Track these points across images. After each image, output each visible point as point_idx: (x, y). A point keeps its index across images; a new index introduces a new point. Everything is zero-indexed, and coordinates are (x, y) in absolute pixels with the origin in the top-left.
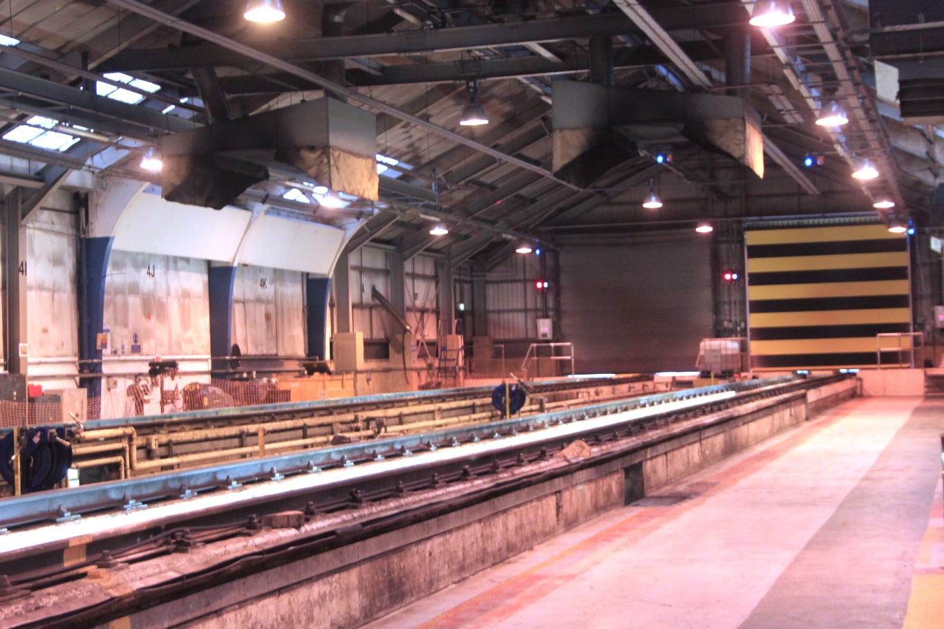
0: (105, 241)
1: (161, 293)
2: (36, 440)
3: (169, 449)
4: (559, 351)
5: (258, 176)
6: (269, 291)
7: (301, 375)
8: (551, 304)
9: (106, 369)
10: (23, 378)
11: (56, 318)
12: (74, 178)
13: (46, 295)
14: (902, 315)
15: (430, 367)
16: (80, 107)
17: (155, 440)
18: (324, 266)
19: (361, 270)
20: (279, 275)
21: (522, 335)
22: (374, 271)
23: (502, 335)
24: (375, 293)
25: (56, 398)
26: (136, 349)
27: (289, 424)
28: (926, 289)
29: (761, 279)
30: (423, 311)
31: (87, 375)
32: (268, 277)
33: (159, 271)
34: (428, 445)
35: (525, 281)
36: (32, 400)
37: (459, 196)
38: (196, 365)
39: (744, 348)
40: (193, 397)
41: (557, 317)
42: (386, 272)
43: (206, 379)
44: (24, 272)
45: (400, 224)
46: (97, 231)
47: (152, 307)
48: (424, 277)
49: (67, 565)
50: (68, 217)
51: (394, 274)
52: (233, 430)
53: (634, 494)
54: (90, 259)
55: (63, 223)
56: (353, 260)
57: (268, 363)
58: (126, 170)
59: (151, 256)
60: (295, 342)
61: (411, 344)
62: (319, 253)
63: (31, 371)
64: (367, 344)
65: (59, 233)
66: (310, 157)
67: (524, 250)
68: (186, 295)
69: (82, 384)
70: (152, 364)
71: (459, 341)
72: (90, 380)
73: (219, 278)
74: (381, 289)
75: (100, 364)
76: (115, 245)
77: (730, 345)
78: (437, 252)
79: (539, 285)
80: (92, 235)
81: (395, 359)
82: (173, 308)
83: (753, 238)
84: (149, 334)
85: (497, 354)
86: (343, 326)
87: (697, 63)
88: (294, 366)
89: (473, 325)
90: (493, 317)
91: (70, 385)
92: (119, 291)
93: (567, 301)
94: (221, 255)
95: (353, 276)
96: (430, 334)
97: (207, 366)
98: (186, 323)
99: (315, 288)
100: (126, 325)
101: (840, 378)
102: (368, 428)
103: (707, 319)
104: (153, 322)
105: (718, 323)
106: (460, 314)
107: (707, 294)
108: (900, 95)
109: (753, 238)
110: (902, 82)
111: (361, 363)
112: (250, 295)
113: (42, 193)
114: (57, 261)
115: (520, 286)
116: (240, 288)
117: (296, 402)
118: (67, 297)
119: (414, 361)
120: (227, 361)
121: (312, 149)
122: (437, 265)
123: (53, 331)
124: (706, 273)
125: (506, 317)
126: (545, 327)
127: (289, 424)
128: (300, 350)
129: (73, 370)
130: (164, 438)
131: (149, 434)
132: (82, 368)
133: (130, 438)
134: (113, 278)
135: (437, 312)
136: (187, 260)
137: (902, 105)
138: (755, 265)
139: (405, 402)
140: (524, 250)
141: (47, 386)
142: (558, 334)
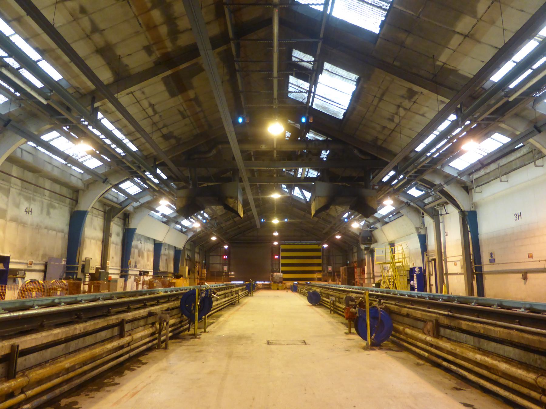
1: (143, 249)
8: (227, 262)
10: (108, 273)
11: (116, 254)
14: (320, 268)
18: (180, 246)
26: (136, 267)
28: (325, 262)
31: (124, 274)
34: (113, 297)
35: (220, 256)
36: (109, 281)
41: (229, 265)
42: (190, 250)
44: (111, 236)
46: (132, 226)
50: (122, 220)
54: (128, 236)
55: (120, 222)
57: (166, 273)
60: (171, 269)
65: (119, 226)
68: (149, 251)
69: (122, 277)
70: (140, 272)
72: (124, 275)
73: (158, 246)
75: (128, 270)
76: (137, 232)
79: (225, 257)
80: (130, 227)
84: (139, 263)
87: (236, 209)
90: (211, 265)
91: (117, 277)
94: (160, 238)
98: (148, 260)
102: (232, 295)
104: (140, 258)
105: (272, 269)
116: (163, 251)
118: (119, 247)
121: (232, 198)
123: (115, 258)
125: (214, 265)
126: (226, 268)
128: (172, 271)
129: (119, 272)
131: (411, 301)
132: (122, 271)
135: (199, 263)
138: (283, 254)
141: (113, 277)
142: (229, 270)
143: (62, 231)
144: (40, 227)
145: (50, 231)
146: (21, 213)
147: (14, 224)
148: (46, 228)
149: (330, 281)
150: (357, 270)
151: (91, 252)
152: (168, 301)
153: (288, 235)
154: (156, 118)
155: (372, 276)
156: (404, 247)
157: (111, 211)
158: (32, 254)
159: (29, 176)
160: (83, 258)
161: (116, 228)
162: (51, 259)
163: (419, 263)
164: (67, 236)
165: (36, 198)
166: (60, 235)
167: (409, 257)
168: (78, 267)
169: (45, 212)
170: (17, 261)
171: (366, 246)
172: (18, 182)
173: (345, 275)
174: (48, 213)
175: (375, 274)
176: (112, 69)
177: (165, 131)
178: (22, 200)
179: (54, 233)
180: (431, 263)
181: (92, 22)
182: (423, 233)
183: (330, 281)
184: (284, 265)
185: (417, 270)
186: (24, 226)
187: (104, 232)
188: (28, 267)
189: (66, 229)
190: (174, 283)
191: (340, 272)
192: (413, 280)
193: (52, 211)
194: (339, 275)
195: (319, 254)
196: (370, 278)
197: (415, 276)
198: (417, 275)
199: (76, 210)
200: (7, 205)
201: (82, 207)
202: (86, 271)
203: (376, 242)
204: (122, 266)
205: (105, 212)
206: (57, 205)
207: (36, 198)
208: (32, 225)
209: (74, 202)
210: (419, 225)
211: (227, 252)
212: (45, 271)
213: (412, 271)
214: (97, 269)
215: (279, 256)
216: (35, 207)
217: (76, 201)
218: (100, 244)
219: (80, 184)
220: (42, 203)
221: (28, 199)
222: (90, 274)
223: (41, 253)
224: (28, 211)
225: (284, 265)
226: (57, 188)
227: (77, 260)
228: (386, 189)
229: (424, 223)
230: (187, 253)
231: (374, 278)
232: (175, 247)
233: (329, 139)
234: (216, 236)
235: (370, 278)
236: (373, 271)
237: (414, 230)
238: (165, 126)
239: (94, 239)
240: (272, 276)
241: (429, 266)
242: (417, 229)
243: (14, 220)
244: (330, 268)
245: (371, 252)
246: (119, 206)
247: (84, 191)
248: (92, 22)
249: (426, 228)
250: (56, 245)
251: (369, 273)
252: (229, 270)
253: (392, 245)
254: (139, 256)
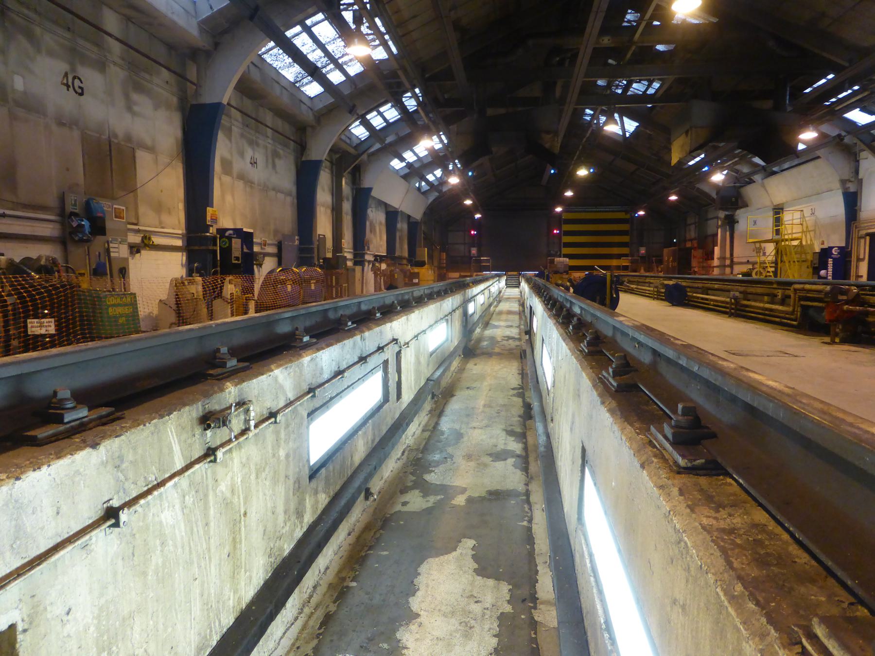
14: (625, 251)
29: (567, 233)
46: (366, 184)
54: (362, 199)
68: (381, 223)
75: (364, 254)
80: (362, 186)
98: (381, 237)
104: (372, 236)
121: (548, 132)
126: (474, 251)
138: (566, 227)
142: (480, 254)
143: (290, 194)
147: (240, 184)
149: (642, 271)
150: (697, 253)
151: (323, 226)
153: (589, 192)
155: (728, 262)
156: (807, 213)
163: (837, 240)
167: (814, 231)
169: (270, 166)
171: (727, 213)
173: (673, 261)
174: (274, 166)
175: (735, 260)
180: (862, 241)
182: (852, 188)
183: (642, 271)
184: (567, 245)
185: (834, 252)
186: (251, 187)
188: (262, 248)
189: (294, 190)
190: (418, 273)
191: (662, 256)
192: (826, 268)
193: (277, 161)
194: (660, 262)
195: (625, 227)
196: (725, 266)
197: (830, 261)
198: (835, 260)
199: (303, 159)
200: (231, 154)
203: (746, 205)
206: (281, 152)
207: (260, 142)
210: (847, 173)
213: (825, 253)
217: (302, 147)
219: (308, 116)
225: (567, 245)
226: (280, 124)
228: (815, 109)
229: (857, 172)
231: (731, 266)
232: (409, 217)
233: (368, 6)
235: (725, 266)
236: (732, 254)
237: (837, 185)
240: (552, 262)
241: (858, 245)
242: (843, 182)
243: (241, 177)
244: (643, 251)
245: (731, 222)
246: (352, 151)
247: (313, 127)
249: (860, 182)
251: (722, 258)
252: (480, 254)
253: (778, 210)
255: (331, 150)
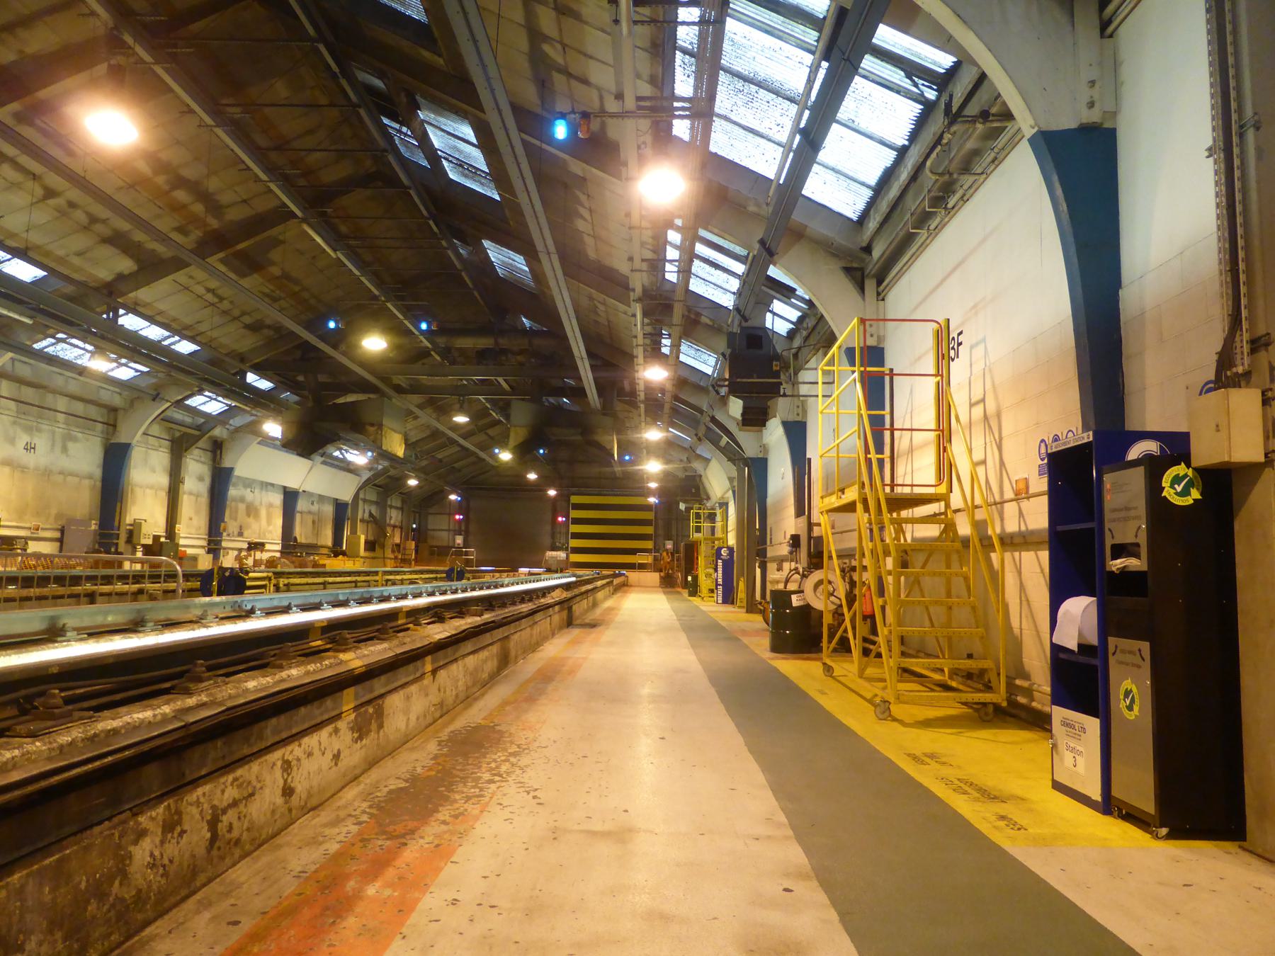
0: (231, 469)
1: (257, 503)
2: (227, 574)
3: (288, 588)
4: (467, 553)
5: (333, 439)
6: (315, 508)
7: (329, 556)
9: (224, 544)
10: (177, 545)
11: (197, 512)
12: (218, 432)
13: (193, 498)
14: (649, 545)
15: (396, 558)
16: (236, 389)
17: (282, 581)
18: (346, 496)
19: (365, 501)
20: (322, 498)
21: (445, 544)
22: (371, 502)
23: (434, 544)
24: (371, 515)
25: (194, 559)
26: (241, 534)
27: (349, 579)
28: (661, 532)
29: (577, 521)
30: (394, 527)
32: (315, 499)
33: (257, 491)
35: (449, 514)
37: (424, 463)
38: (274, 547)
39: (567, 557)
40: (271, 563)
42: (376, 503)
43: (278, 555)
45: (389, 477)
46: (226, 463)
47: (252, 510)
48: (396, 508)
49: (400, 622)
51: (382, 504)
52: (320, 580)
53: (569, 623)
54: (220, 480)
56: (361, 496)
57: (312, 548)
58: (252, 429)
59: (254, 481)
60: (327, 538)
61: (389, 543)
62: (345, 489)
63: (182, 542)
64: (366, 542)
65: (203, 463)
66: (371, 429)
67: (453, 497)
68: (270, 505)
69: (209, 552)
71: (413, 545)
73: (290, 497)
74: (373, 512)
76: (237, 473)
77: (561, 555)
78: (407, 495)
81: (378, 552)
82: (263, 513)
83: (575, 499)
85: (432, 553)
86: (354, 531)
88: (325, 551)
89: (420, 536)
91: (201, 552)
92: (235, 500)
93: (472, 528)
94: (293, 484)
95: (361, 503)
96: (397, 540)
97: (279, 547)
98: (269, 522)
99: (340, 507)
100: (236, 520)
101: (615, 576)
103: (547, 540)
104: (251, 520)
106: (413, 530)
107: (548, 528)
108: (743, 415)
109: (575, 499)
110: (745, 408)
111: (362, 552)
112: (305, 509)
113: (198, 438)
114: (201, 479)
115: (446, 517)
116: (302, 505)
117: (328, 569)
118: (204, 500)
119: (389, 554)
120: (289, 544)
121: (372, 425)
122: (403, 502)
124: (549, 516)
126: (459, 540)
127: (349, 579)
128: (330, 543)
129: (204, 543)
130: (286, 581)
132: (210, 542)
133: (270, 579)
134: (233, 492)
135: (401, 528)
136: (272, 485)
137: (744, 420)
138: (575, 514)
139: (404, 573)
140: (453, 497)
141: (190, 551)
142: (466, 545)
144: (51, 471)
145: (69, 478)
146: (18, 451)
148: (61, 473)
151: (145, 510)
152: (461, 615)
154: (225, 305)
157: (183, 439)
158: (38, 514)
159: (28, 393)
160: (129, 520)
161: (196, 471)
162: (72, 521)
164: (99, 484)
165: (44, 427)
166: (86, 482)
168: (118, 535)
170: (14, 524)
172: (12, 404)
174: (65, 449)
176: (132, 257)
177: (247, 320)
178: (19, 431)
179: (77, 479)
181: (87, 213)
187: (171, 476)
189: (98, 473)
193: (70, 445)
198: (724, 561)
201: (122, 438)
202: (135, 541)
204: (210, 534)
205: (172, 441)
206: (80, 435)
208: (36, 469)
209: (111, 428)
211: (460, 508)
212: (61, 540)
214: (156, 538)
215: (567, 516)
216: (41, 442)
218: (163, 496)
220: (53, 433)
221: (29, 430)
222: (143, 546)
223: (54, 511)
224: (30, 448)
226: (79, 408)
227: (116, 524)
230: (363, 511)
234: (417, 477)
238: (244, 314)
239: (151, 487)
248: (87, 213)
250: (81, 500)
254: (248, 515)
255: (822, 316)
